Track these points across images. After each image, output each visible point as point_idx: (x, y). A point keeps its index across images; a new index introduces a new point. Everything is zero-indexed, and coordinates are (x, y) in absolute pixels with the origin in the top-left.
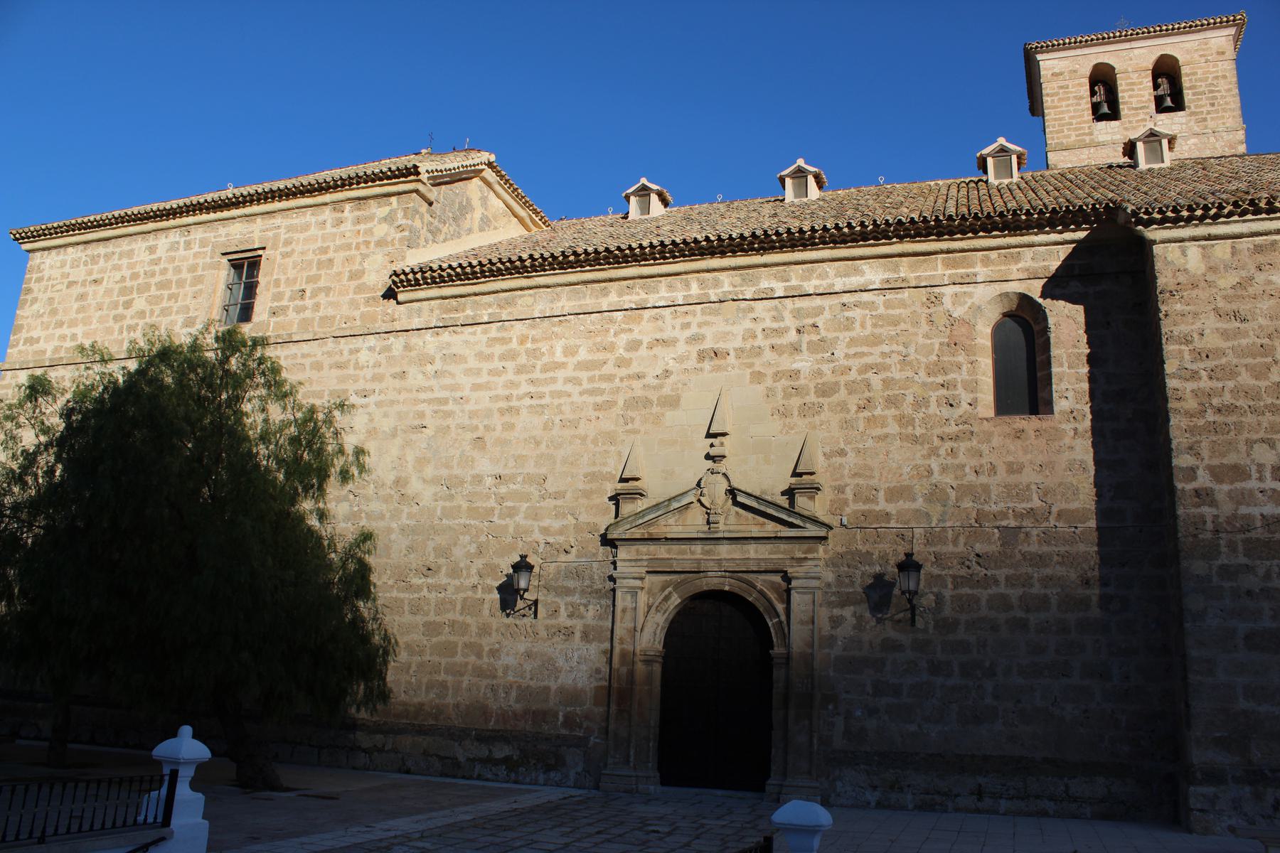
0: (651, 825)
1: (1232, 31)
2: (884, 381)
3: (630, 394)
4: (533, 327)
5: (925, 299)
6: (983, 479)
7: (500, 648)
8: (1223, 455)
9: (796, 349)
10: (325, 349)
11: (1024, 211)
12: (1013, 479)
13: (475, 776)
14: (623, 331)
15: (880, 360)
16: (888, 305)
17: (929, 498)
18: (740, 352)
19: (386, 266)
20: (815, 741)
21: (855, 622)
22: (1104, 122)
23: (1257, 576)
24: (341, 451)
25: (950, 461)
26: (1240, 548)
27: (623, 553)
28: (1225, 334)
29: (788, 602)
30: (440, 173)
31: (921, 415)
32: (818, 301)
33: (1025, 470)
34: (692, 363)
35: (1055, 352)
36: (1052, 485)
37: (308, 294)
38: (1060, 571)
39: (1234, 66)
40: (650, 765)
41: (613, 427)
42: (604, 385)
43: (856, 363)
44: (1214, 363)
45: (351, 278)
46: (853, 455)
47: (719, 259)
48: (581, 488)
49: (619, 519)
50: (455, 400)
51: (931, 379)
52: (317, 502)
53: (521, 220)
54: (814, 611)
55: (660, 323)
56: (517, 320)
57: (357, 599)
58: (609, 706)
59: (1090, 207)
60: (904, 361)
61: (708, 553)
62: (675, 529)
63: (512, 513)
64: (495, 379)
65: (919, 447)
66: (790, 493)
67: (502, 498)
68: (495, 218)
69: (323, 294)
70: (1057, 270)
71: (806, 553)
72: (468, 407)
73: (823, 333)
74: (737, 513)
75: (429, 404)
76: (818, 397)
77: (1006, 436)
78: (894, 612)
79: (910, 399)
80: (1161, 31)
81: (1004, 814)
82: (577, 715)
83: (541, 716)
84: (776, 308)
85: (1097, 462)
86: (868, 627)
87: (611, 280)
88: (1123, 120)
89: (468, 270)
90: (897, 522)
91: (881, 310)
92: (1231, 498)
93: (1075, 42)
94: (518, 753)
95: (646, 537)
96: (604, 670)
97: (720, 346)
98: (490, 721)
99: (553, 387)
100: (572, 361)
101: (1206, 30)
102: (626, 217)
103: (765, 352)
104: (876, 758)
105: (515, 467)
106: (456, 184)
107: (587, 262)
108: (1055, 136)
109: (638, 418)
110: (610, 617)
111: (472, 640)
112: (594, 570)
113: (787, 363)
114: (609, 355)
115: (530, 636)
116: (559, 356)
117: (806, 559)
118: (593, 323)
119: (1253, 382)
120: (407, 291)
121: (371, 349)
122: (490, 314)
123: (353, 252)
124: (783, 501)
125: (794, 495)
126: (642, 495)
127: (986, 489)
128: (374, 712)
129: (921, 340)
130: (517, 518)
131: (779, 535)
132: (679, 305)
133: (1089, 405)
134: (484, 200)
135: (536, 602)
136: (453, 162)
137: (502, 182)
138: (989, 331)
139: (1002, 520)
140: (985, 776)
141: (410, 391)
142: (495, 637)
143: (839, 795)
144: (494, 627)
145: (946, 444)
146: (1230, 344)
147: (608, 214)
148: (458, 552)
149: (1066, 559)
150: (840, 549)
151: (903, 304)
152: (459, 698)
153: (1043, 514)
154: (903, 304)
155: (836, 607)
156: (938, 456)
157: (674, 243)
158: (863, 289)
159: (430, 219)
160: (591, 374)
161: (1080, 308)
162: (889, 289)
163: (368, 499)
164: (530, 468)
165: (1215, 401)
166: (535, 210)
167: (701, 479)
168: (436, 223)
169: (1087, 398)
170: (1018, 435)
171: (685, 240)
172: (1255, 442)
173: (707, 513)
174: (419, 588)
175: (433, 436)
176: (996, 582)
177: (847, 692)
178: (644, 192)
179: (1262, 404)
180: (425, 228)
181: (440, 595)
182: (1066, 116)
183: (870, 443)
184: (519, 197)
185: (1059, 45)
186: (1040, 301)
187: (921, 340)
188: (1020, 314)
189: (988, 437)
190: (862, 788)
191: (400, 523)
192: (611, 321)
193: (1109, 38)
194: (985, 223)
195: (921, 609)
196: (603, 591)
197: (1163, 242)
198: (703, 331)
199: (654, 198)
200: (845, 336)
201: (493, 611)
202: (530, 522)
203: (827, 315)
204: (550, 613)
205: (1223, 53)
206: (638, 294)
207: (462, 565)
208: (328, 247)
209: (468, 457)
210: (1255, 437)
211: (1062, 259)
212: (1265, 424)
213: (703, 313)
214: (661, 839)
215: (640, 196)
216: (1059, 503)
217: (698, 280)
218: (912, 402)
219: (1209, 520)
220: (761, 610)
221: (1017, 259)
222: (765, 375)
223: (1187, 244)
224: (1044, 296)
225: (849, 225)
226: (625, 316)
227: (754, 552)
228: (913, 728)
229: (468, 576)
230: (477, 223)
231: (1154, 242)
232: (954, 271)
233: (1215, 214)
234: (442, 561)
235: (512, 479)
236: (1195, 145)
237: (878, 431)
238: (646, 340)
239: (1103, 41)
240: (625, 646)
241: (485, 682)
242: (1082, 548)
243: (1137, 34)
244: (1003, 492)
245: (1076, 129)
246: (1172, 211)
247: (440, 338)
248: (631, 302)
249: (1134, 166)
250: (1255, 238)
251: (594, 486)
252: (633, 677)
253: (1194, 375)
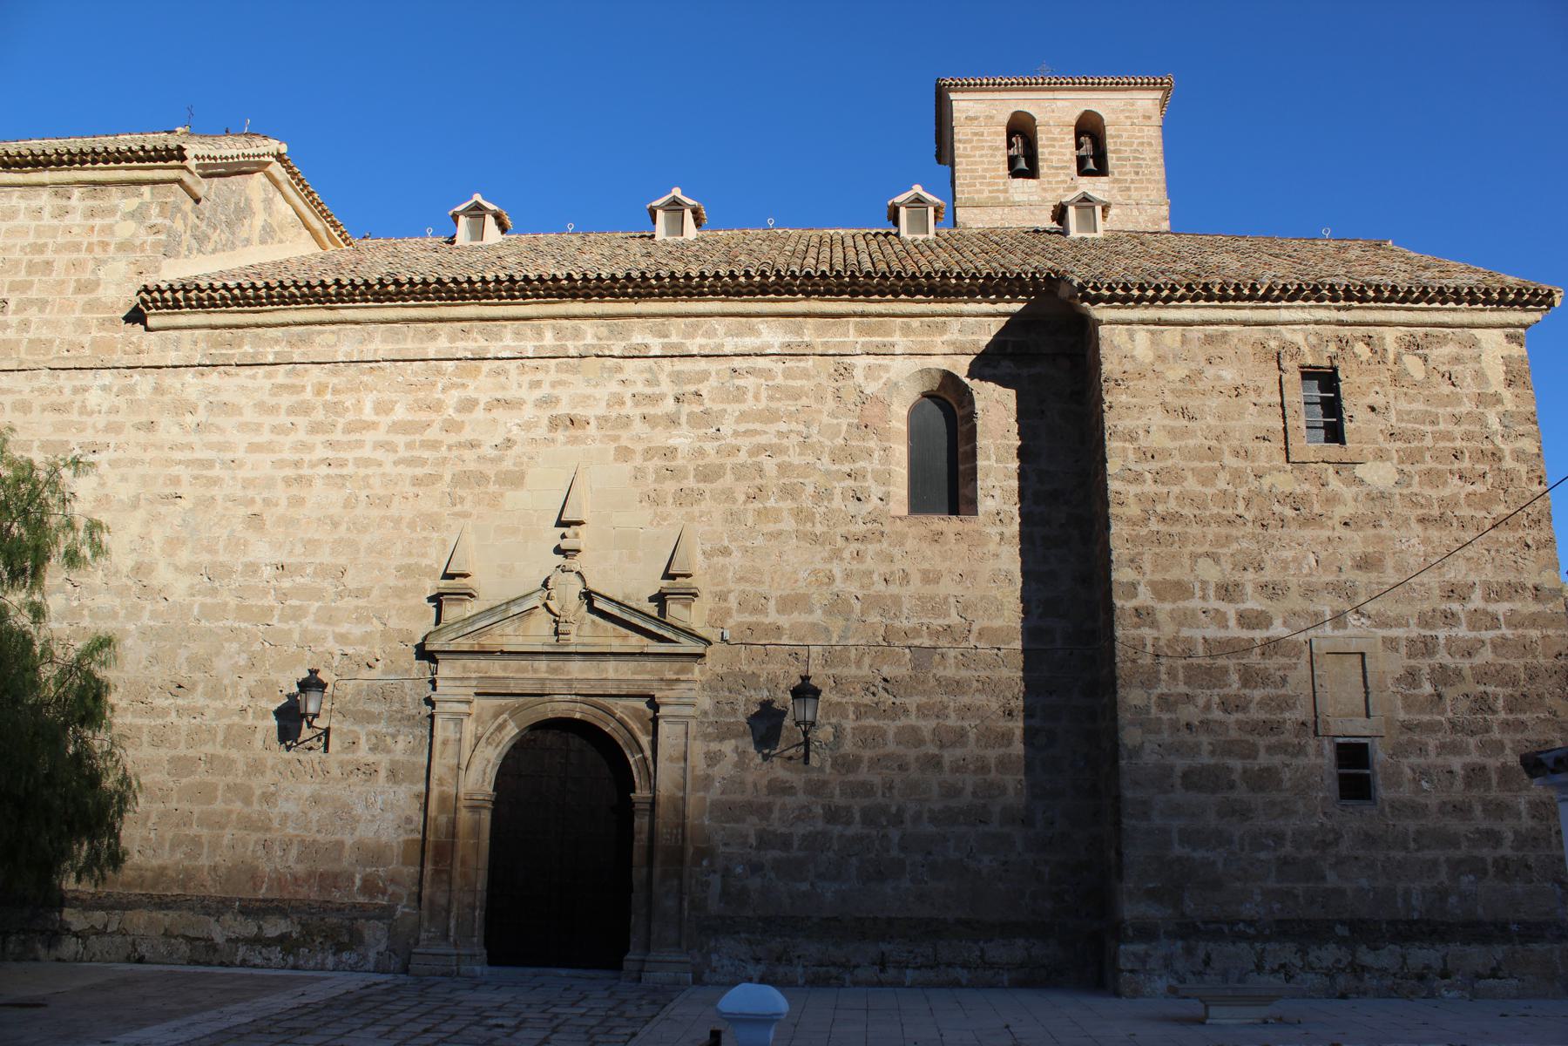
0: (488, 1017)
1: (1159, 95)
2: (779, 466)
3: (459, 468)
4: (335, 373)
5: (832, 371)
6: (894, 589)
7: (277, 791)
8: (1166, 569)
9: (673, 421)
10: (36, 384)
11: (955, 274)
12: (928, 590)
13: (238, 962)
14: (454, 386)
15: (775, 441)
16: (788, 374)
17: (830, 610)
18: (603, 421)
19: (131, 279)
20: (686, 904)
21: (736, 759)
22: (1021, 180)
23: (1197, 706)
24: (70, 525)
25: (855, 566)
26: (1181, 676)
27: (445, 669)
28: (1172, 433)
29: (655, 733)
30: (213, 161)
31: (823, 509)
32: (703, 364)
33: (943, 580)
34: (542, 431)
35: (981, 442)
36: (973, 599)
37: (12, 306)
38: (980, 699)
39: (1160, 134)
40: (475, 939)
41: (436, 509)
42: (426, 454)
43: (746, 443)
44: (1162, 465)
45: (78, 290)
46: (739, 555)
47: (582, 304)
48: (391, 584)
49: (441, 625)
50: (223, 463)
51: (835, 467)
52: (31, 592)
53: (314, 234)
54: (686, 746)
55: (502, 379)
56: (313, 363)
57: (82, 726)
58: (422, 865)
59: (1030, 275)
60: (805, 443)
61: (555, 671)
62: (513, 640)
63: (297, 614)
64: (281, 438)
65: (818, 548)
66: (660, 599)
67: (284, 594)
68: (281, 227)
69: (35, 309)
70: (987, 346)
71: (678, 674)
72: (241, 474)
73: (708, 404)
74: (593, 622)
75: (187, 466)
76: (698, 482)
77: (922, 538)
78: (783, 747)
79: (810, 489)
80: (1086, 83)
81: (908, 987)
82: (380, 877)
83: (329, 880)
84: (650, 370)
85: (1025, 573)
86: (752, 765)
87: (441, 320)
88: (1041, 179)
89: (250, 293)
90: (790, 638)
91: (780, 380)
92: (1172, 618)
93: (994, 84)
94: (299, 928)
95: (476, 649)
97: (579, 412)
98: (261, 888)
99: (358, 453)
100: (385, 421)
101: (1132, 89)
102: (451, 241)
103: (634, 423)
104: (760, 924)
105: (304, 554)
106: (233, 178)
107: (412, 295)
108: (966, 189)
109: (470, 498)
110: (426, 751)
111: (239, 781)
112: (407, 690)
113: (661, 438)
114: (434, 416)
115: (318, 776)
116: (368, 414)
117: (678, 680)
118: (415, 374)
119: (1199, 488)
120: (161, 314)
121: (104, 388)
122: (276, 353)
123: (83, 255)
124: (652, 609)
125: (665, 602)
126: (471, 596)
127: (897, 600)
128: (100, 882)
129: (826, 419)
130: (305, 622)
131: (646, 650)
132: (528, 358)
133: (1018, 506)
134: (268, 202)
135: (327, 731)
136: (231, 148)
137: (293, 182)
138: (905, 413)
139: (914, 638)
140: (889, 943)
141: (161, 447)
142: (270, 776)
143: (715, 971)
144: (270, 763)
145: (851, 546)
146: (1177, 444)
147: (427, 236)
148: (221, 665)
149: (987, 686)
150: (719, 670)
151: (805, 374)
152: (218, 858)
153: (962, 633)
154: (805, 374)
155: (714, 740)
156: (842, 559)
157: (526, 279)
158: (758, 353)
159: (196, 221)
160: (409, 438)
161: (1012, 393)
162: (790, 355)
163: (93, 591)
164: (325, 557)
165: (1160, 508)
166: (334, 222)
167: (548, 578)
168: (203, 226)
169: (1016, 499)
170: (936, 538)
171: (540, 276)
172: (1200, 556)
173: (555, 621)
174: (165, 712)
175: (191, 509)
176: (906, 712)
177: (726, 845)
178: (477, 212)
179: (1208, 513)
180: (189, 232)
181: (194, 721)
182: (980, 168)
183: (760, 541)
184: (314, 204)
185: (975, 85)
186: (967, 381)
187: (826, 419)
188: (942, 394)
189: (901, 539)
190: (743, 961)
191: (139, 624)
192: (439, 372)
193: (1031, 84)
194: (908, 285)
195: (817, 744)
196: (418, 717)
197: (1110, 323)
198: (557, 392)
199: (490, 221)
200: (734, 409)
201: (267, 742)
202: (322, 627)
203: (713, 381)
204: (346, 745)
205: (1149, 118)
206: (475, 340)
207: (226, 682)
208: (45, 245)
209: (239, 539)
210: (1200, 550)
211: (993, 333)
212: (1210, 537)
213: (558, 369)
214: (509, 1035)
215: (471, 216)
216: (980, 620)
217: (554, 327)
218: (812, 493)
219: (1149, 642)
220: (621, 743)
221: (942, 329)
222: (633, 451)
223: (1135, 327)
224: (971, 375)
225: (747, 274)
226: (457, 367)
227: (612, 671)
228: (805, 887)
229: (235, 696)
230: (257, 231)
231: (1100, 322)
232: (867, 339)
233: (1278, 295)
234: (198, 676)
235: (299, 569)
236: (1117, 216)
237: (771, 527)
238: (484, 399)
239: (1025, 87)
241: (254, 836)
242: (1005, 673)
243: (1062, 84)
244: (916, 605)
245: (989, 184)
246: (1122, 289)
247: (205, 380)
248: (465, 349)
249: (1065, 233)
250: (1206, 327)
251: (409, 582)
252: (454, 827)
253: (1138, 478)
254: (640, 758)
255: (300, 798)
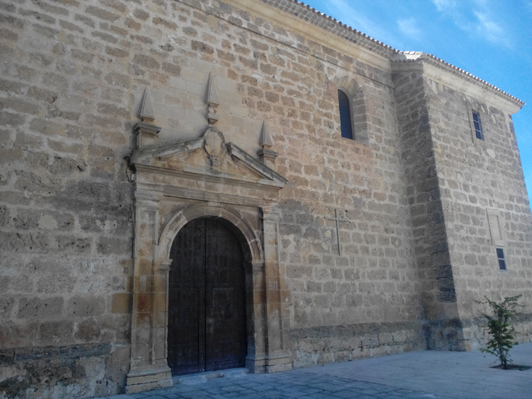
3: (138, 52)
15: (297, 90)
42: (116, 36)
77: (353, 150)
82: (94, 323)
91: (297, 61)
96: (121, 279)
99: (64, 18)
130: (21, 127)
160: (103, 21)
202: (38, 134)
204: (62, 224)
220: (243, 232)
227: (239, 191)
228: (327, 310)
240: (144, 257)
251: (108, 116)
252: (152, 284)
254: (253, 242)
255: (21, 265)
